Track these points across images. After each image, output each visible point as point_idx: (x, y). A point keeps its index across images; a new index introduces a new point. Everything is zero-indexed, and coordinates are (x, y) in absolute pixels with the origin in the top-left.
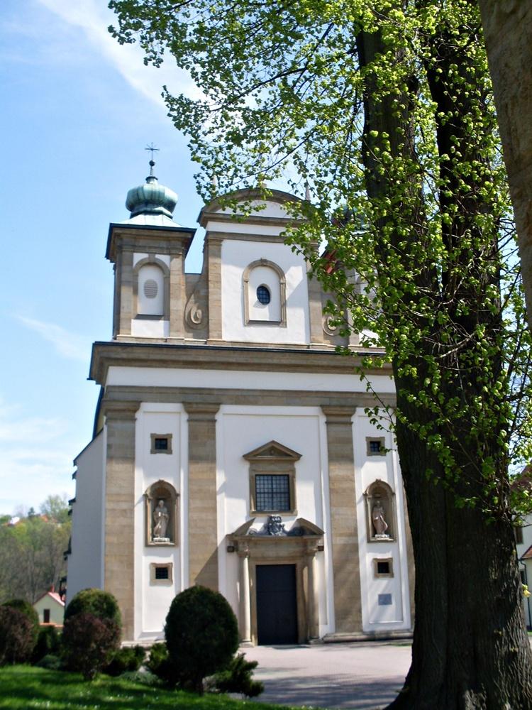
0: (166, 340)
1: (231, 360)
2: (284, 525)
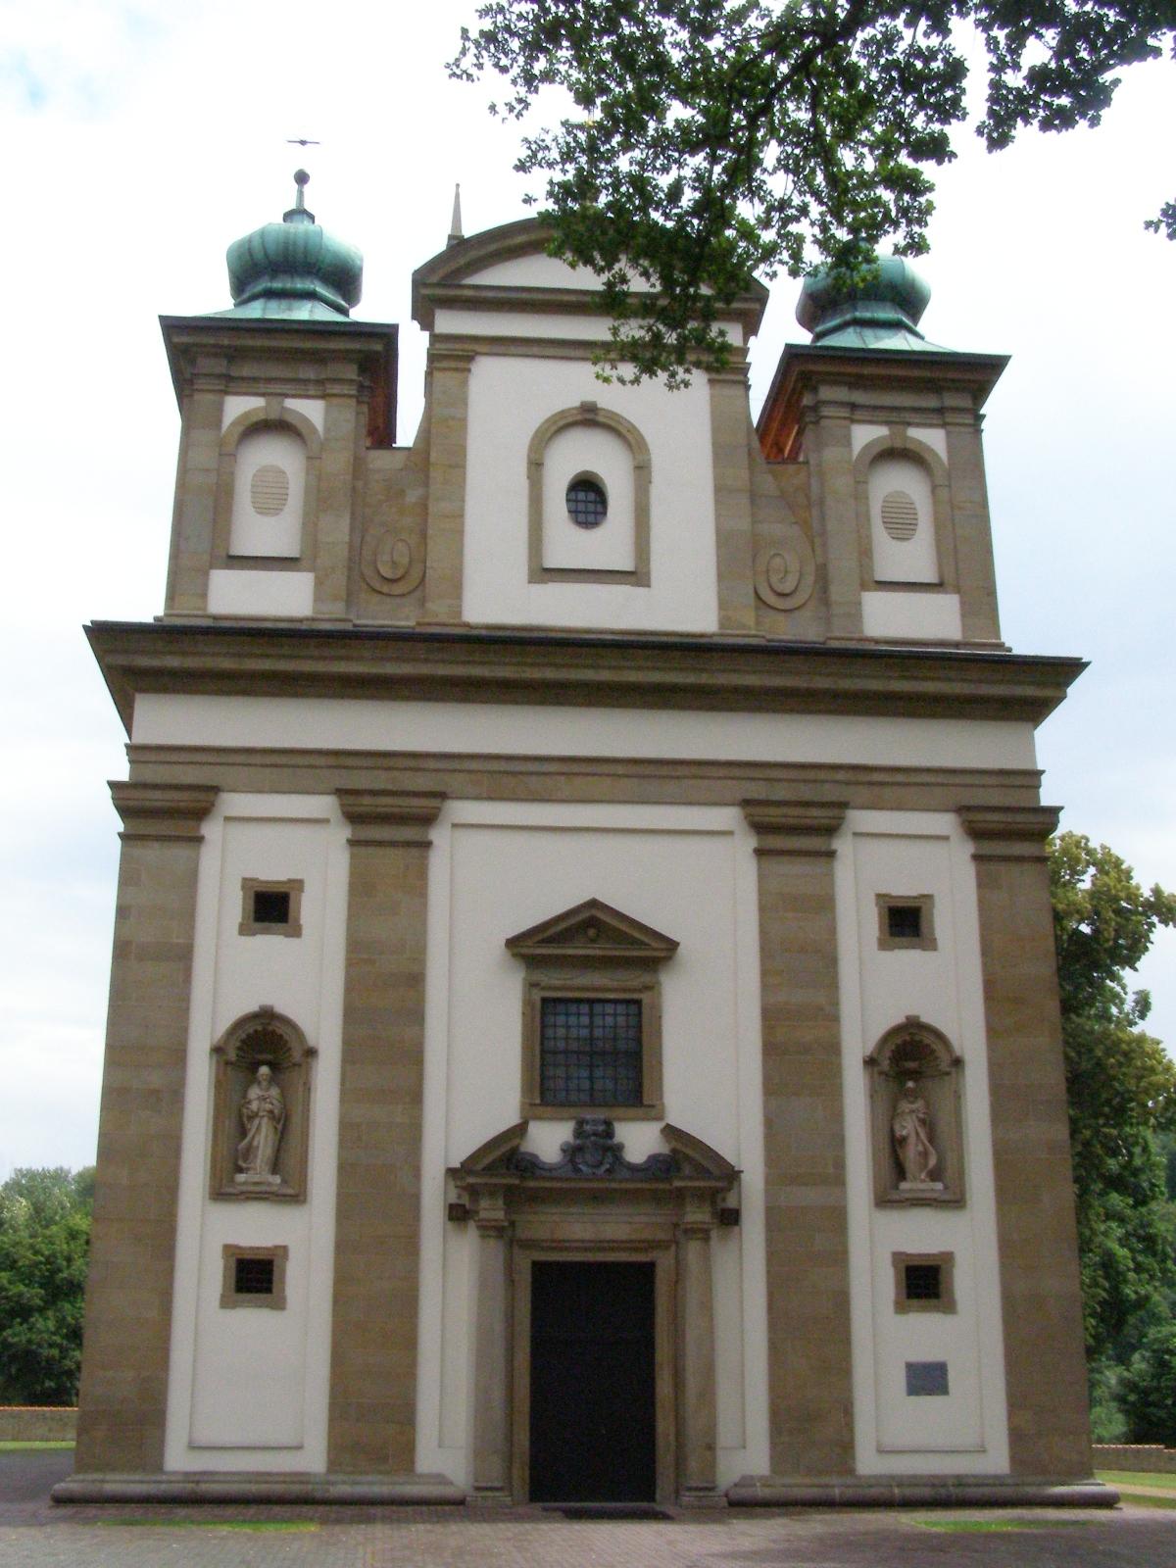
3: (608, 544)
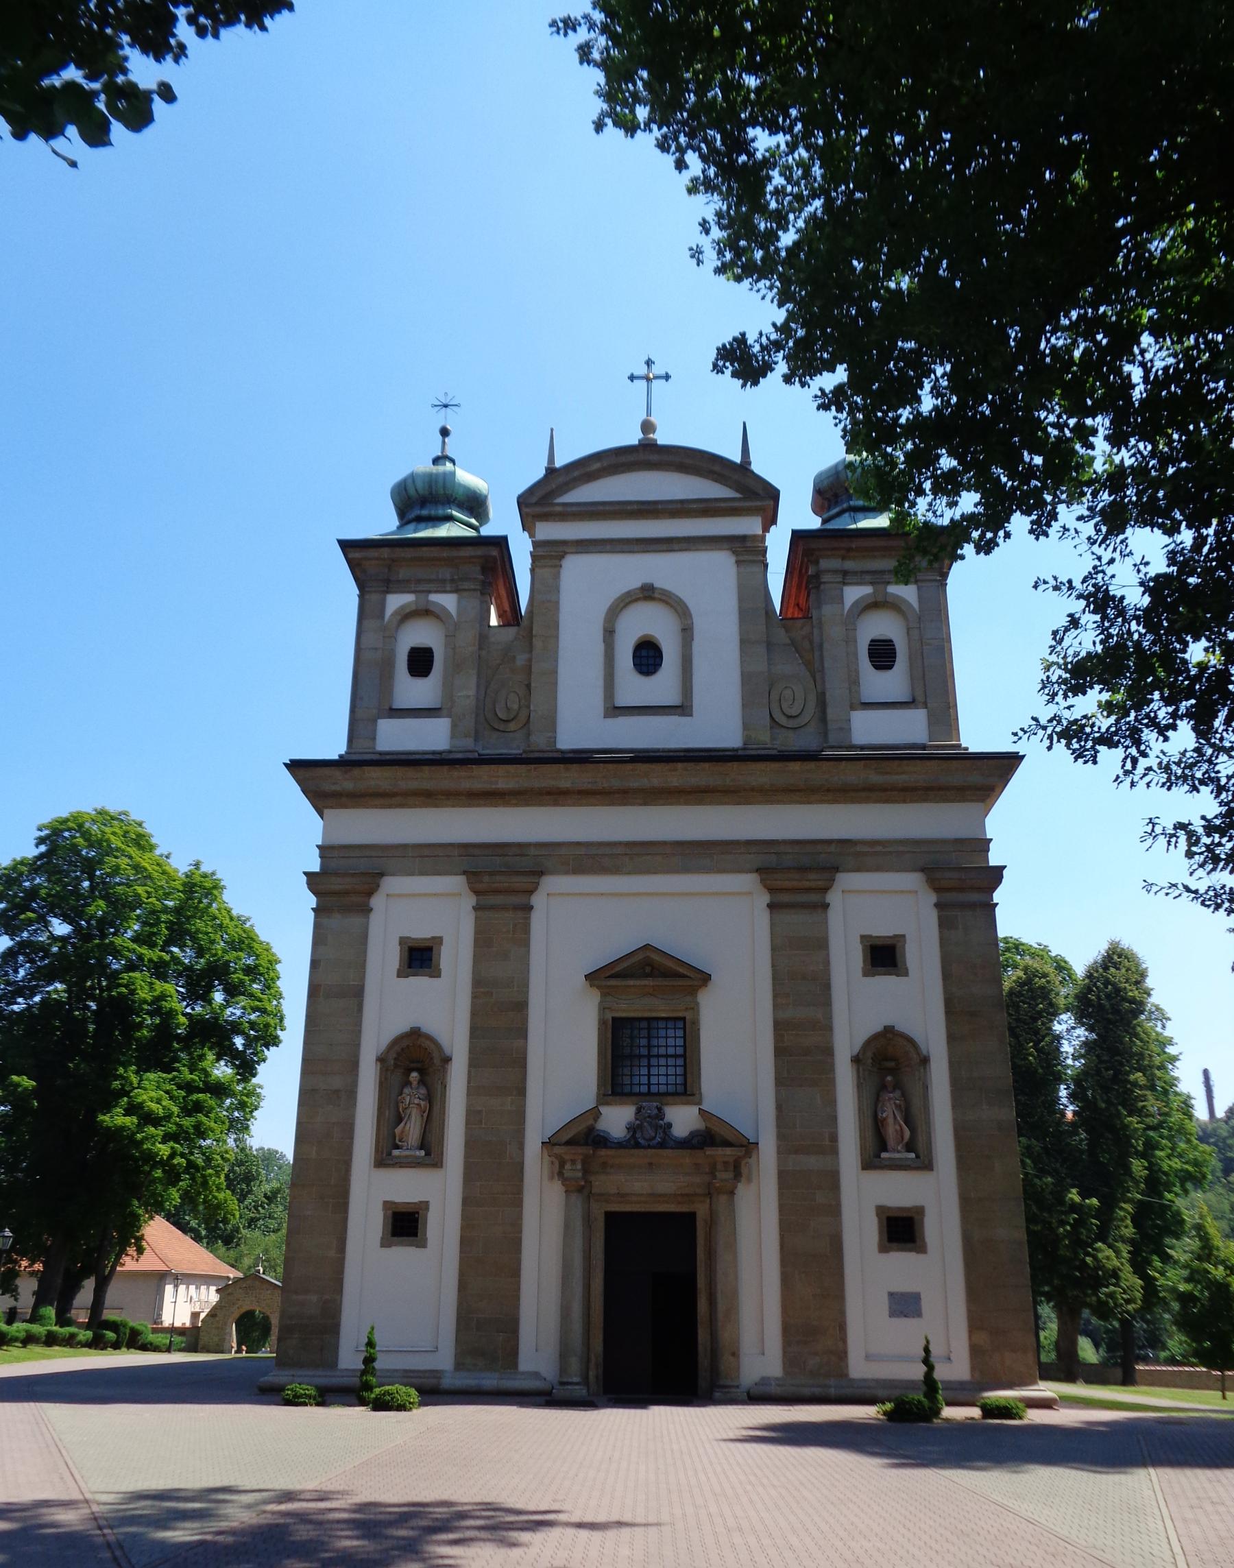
3: (662, 686)
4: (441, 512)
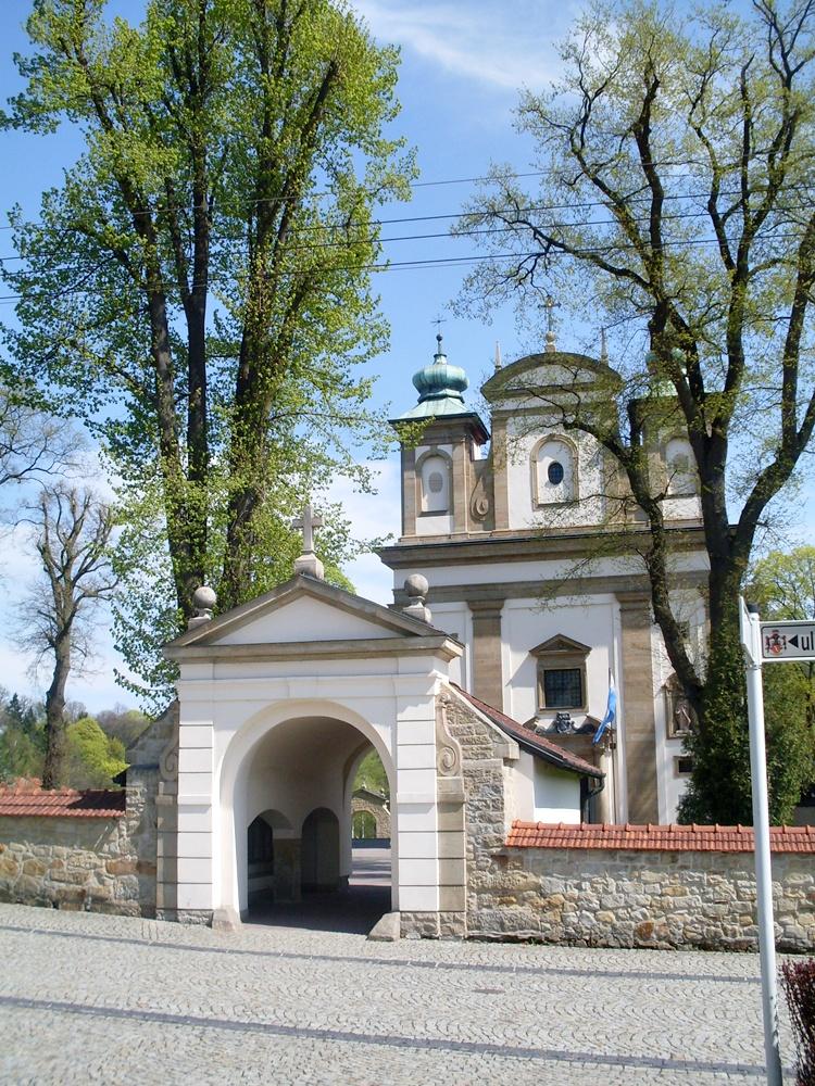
0: (450, 536)
1: (513, 552)
2: (573, 723)
4: (440, 393)
